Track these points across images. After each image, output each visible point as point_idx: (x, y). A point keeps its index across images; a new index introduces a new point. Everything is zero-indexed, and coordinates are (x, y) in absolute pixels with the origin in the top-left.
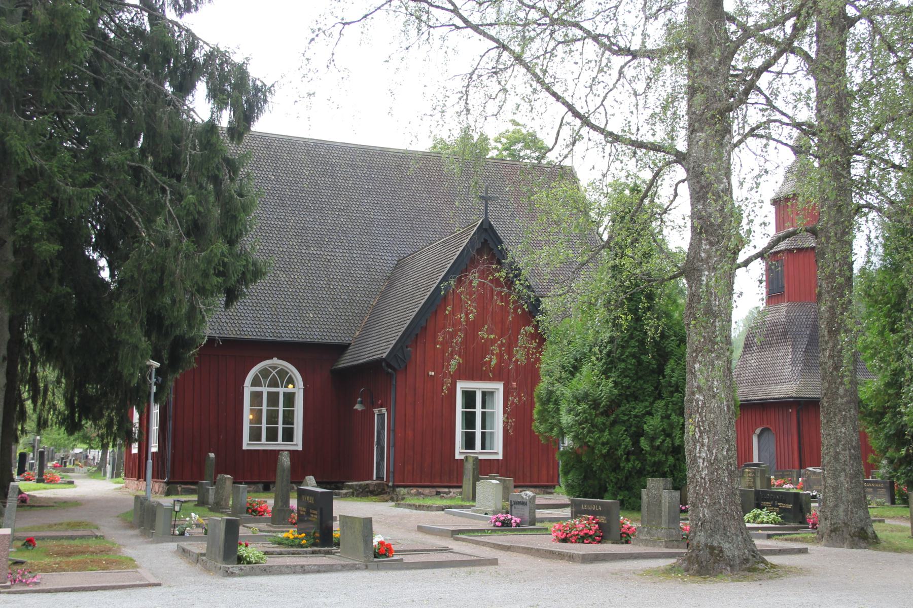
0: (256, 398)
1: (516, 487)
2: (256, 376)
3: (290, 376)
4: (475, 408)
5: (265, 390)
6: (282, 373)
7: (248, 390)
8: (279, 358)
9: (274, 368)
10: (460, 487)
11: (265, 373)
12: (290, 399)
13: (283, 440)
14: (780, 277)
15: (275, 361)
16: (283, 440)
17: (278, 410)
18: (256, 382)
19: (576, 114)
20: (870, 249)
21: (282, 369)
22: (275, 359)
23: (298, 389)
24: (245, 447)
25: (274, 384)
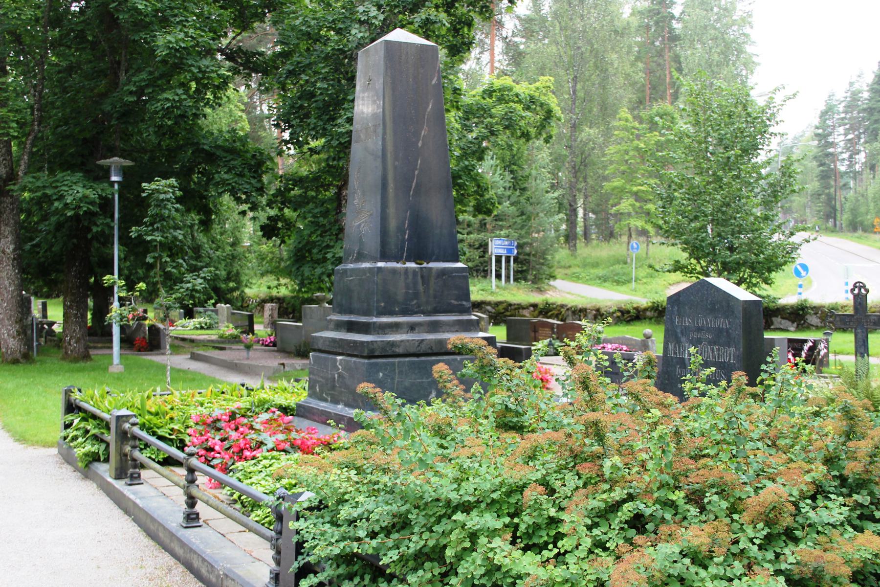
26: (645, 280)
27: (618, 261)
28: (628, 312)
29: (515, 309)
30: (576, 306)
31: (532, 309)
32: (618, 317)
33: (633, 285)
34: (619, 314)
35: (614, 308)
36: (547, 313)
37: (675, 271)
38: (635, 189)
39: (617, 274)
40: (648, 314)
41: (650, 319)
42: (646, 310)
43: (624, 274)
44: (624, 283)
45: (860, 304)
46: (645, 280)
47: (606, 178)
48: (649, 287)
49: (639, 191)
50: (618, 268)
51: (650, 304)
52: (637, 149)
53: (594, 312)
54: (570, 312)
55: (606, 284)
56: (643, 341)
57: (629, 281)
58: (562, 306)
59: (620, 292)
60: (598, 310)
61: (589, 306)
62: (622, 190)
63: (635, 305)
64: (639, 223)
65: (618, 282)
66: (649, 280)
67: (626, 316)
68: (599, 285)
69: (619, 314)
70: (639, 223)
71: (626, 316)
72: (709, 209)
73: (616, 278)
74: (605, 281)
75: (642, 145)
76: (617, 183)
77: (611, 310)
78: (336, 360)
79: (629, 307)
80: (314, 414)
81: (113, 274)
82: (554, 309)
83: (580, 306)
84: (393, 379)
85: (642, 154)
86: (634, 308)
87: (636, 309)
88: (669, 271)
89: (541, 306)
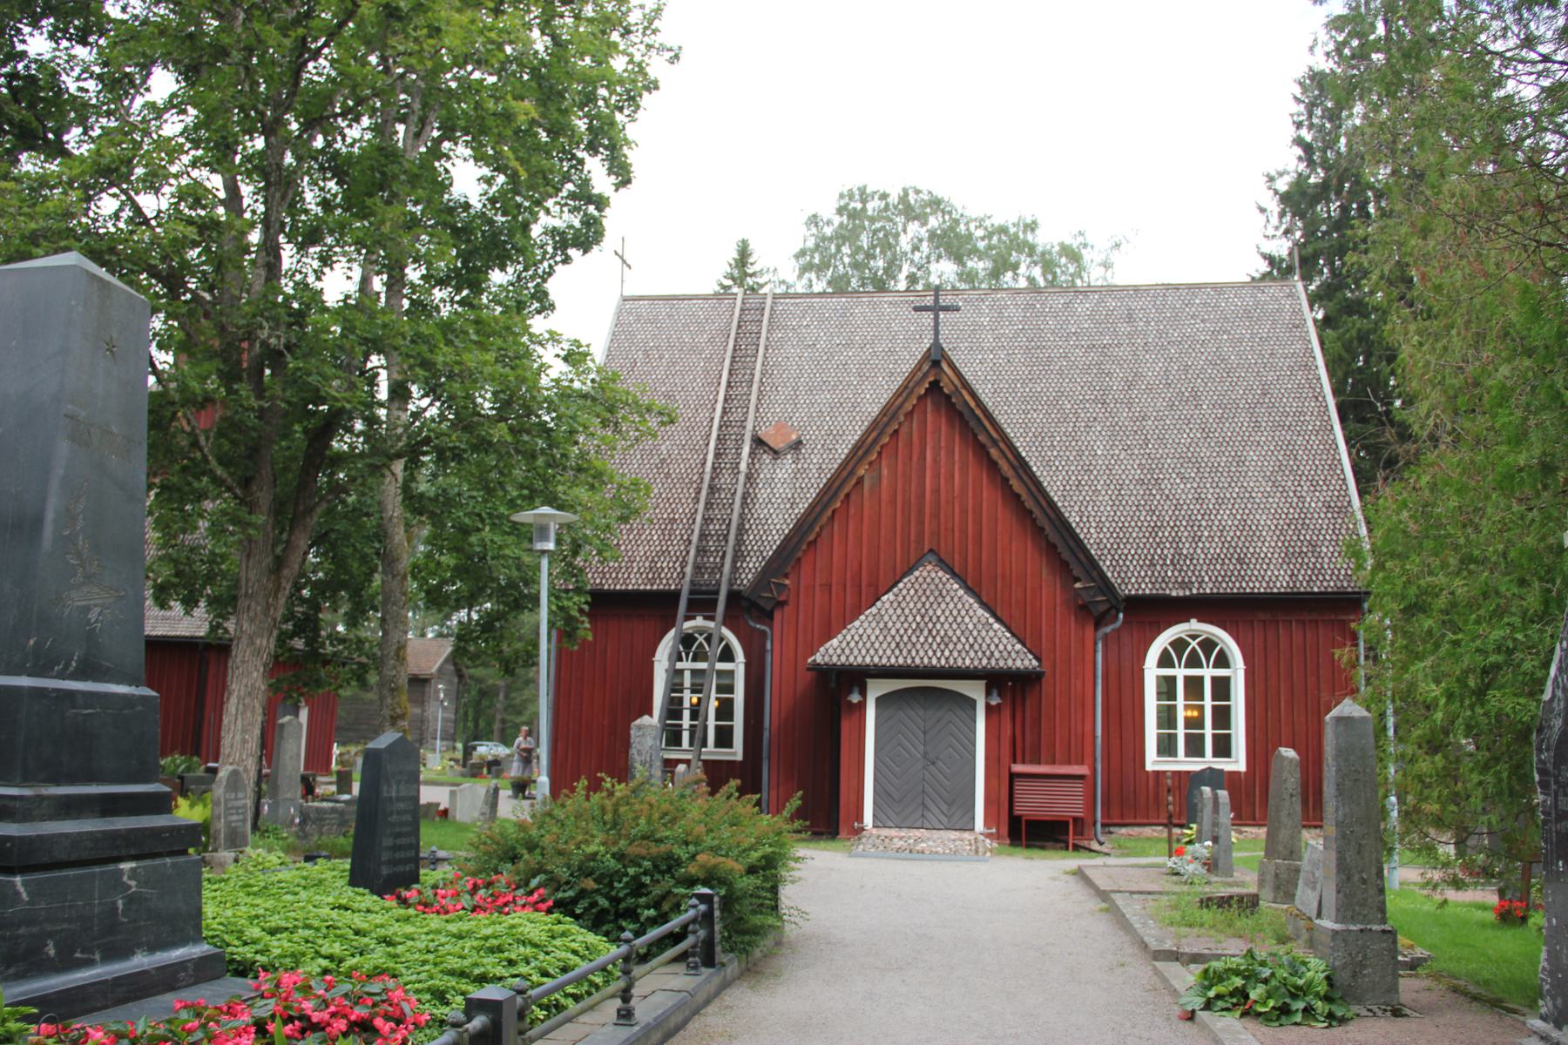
0: (1167, 687)
1: (1304, 826)
2: (1165, 651)
3: (1221, 650)
4: (732, 720)
5: (1180, 673)
6: (1208, 645)
7: (1152, 672)
8: (1200, 621)
9: (1194, 637)
10: (1321, 827)
11: (1179, 645)
12: (1222, 688)
13: (1187, 755)
14: (1021, 471)
15: (1195, 625)
16: (1187, 755)
17: (717, 720)
18: (1165, 661)
19: (127, 41)
20: (412, 357)
21: (1207, 639)
22: (1193, 621)
23: (1237, 673)
24: (1149, 767)
25: (1194, 662)
78: (121, 872)
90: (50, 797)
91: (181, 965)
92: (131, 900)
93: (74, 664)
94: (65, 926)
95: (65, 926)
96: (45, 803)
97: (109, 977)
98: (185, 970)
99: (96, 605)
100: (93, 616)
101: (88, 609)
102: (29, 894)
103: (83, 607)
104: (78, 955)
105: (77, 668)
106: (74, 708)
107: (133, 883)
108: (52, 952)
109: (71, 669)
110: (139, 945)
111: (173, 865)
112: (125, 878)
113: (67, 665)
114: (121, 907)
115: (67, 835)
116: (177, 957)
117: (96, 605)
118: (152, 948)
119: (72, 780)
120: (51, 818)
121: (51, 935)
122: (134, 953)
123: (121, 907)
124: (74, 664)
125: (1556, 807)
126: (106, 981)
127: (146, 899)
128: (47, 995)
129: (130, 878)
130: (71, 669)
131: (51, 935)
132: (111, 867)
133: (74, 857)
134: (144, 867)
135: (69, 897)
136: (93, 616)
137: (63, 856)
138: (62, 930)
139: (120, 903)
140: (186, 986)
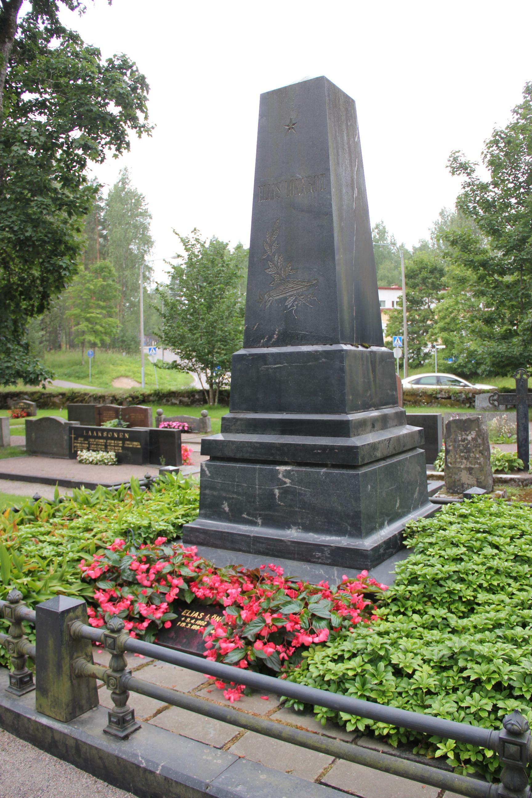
26: (97, 376)
27: (77, 364)
28: (137, 397)
29: (48, 397)
30: (97, 394)
31: (61, 397)
32: (130, 401)
33: (90, 379)
34: (131, 399)
35: (127, 395)
36: (73, 399)
37: (172, 368)
38: (88, 315)
39: (77, 372)
40: (151, 398)
41: (153, 402)
42: (150, 395)
43: (82, 372)
44: (83, 378)
45: (522, 386)
46: (97, 376)
47: (68, 308)
48: (101, 381)
49: (91, 317)
50: (77, 368)
51: (152, 392)
52: (88, 289)
53: (111, 398)
54: (92, 399)
55: (71, 379)
56: (201, 419)
57: (87, 376)
58: (86, 394)
59: (82, 384)
60: (114, 397)
61: (106, 394)
62: (77, 316)
63: (142, 393)
64: (92, 338)
65: (79, 378)
66: (101, 375)
67: (136, 400)
68: (66, 380)
69: (131, 399)
70: (91, 338)
71: (136, 400)
72: (203, 325)
73: (77, 375)
74: (70, 376)
75: (92, 287)
76: (76, 311)
77: (125, 397)
78: (277, 472)
79: (137, 394)
80: (233, 542)
81: (245, 347)
82: (79, 396)
83: (100, 394)
84: (376, 491)
85: (93, 293)
86: (141, 395)
87: (143, 395)
88: (168, 368)
89: (69, 395)
90: (241, 420)
91: (319, 547)
92: (285, 492)
93: (275, 336)
94: (235, 496)
95: (235, 496)
96: (239, 422)
97: (252, 535)
98: (322, 551)
99: (291, 296)
100: (289, 303)
101: (285, 299)
102: (210, 472)
103: (280, 299)
104: (245, 516)
105: (278, 339)
106: (265, 365)
107: (287, 480)
108: (227, 509)
109: (273, 340)
110: (296, 524)
111: (325, 473)
112: (280, 476)
113: (270, 338)
114: (277, 495)
115: (233, 442)
116: (323, 541)
117: (291, 296)
118: (307, 528)
119: (266, 410)
120: (243, 432)
121: (226, 499)
122: (289, 528)
123: (277, 495)
124: (275, 336)
125: (199, 375)
126: (249, 536)
127: (300, 494)
128: (208, 530)
129: (284, 476)
130: (273, 340)
131: (226, 499)
132: (271, 467)
133: (238, 456)
134: (296, 471)
135: (237, 480)
136: (289, 303)
137: (231, 454)
138: (233, 498)
139: (277, 492)
140: (321, 563)
